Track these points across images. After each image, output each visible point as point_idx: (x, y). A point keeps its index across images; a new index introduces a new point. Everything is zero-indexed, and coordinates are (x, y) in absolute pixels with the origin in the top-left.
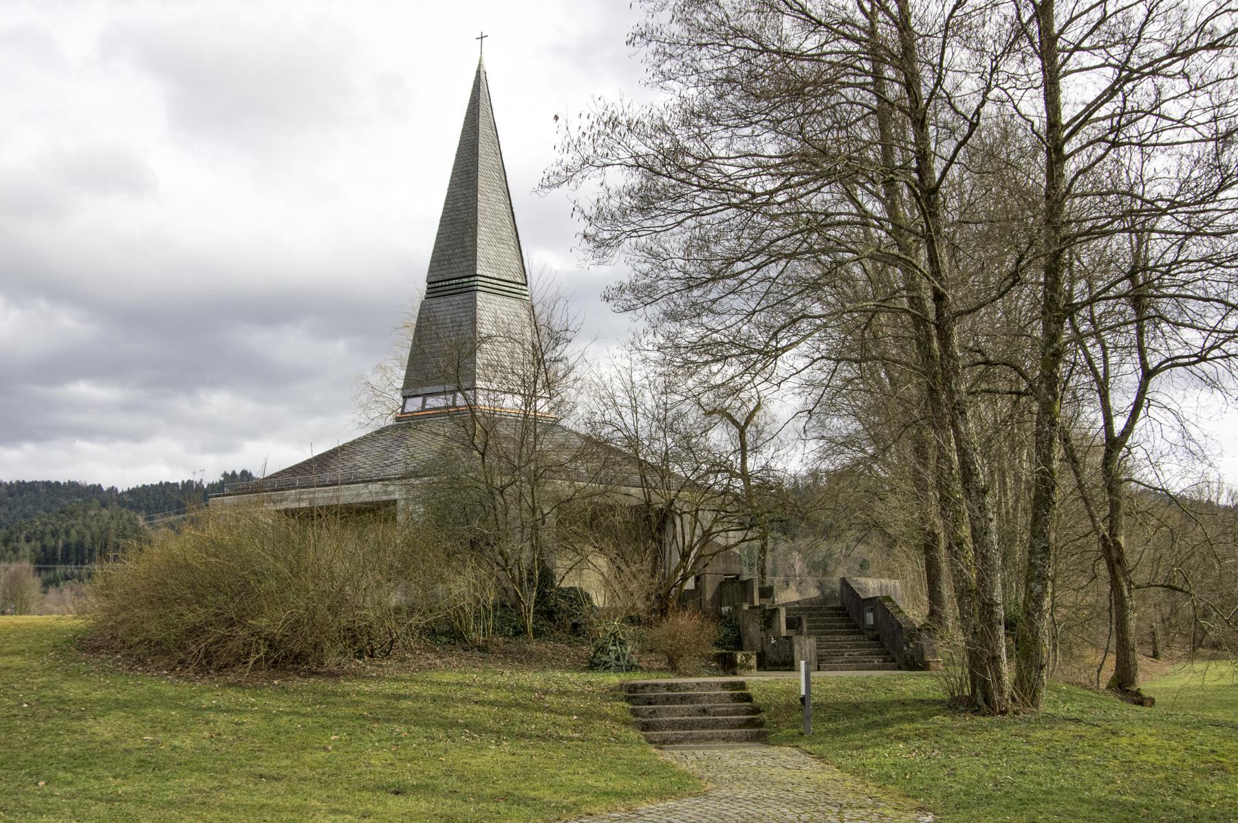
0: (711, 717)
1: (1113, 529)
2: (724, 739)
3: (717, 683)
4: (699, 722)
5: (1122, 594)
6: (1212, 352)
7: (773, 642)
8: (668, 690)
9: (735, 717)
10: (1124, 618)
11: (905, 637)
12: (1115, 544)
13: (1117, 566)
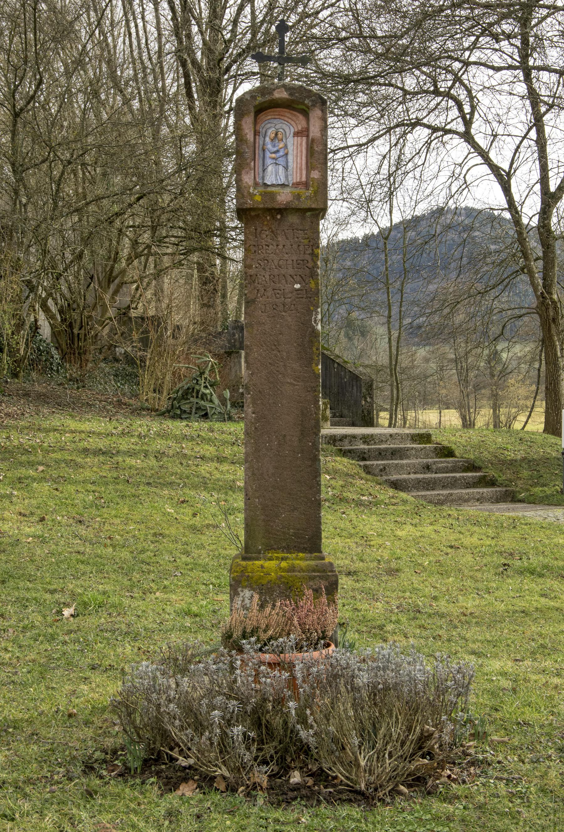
0: (433, 475)
1: (547, 286)
2: (478, 500)
3: (407, 435)
4: (440, 480)
5: (556, 354)
6: (176, 88)
7: (241, 390)
8: (364, 442)
9: (470, 474)
10: (557, 379)
11: (364, 390)
12: (552, 302)
13: (553, 326)
